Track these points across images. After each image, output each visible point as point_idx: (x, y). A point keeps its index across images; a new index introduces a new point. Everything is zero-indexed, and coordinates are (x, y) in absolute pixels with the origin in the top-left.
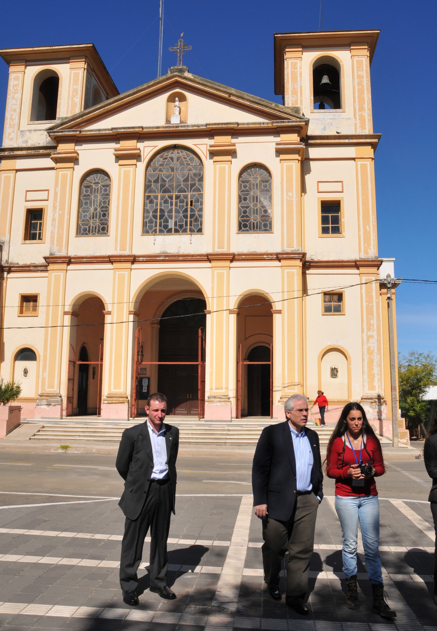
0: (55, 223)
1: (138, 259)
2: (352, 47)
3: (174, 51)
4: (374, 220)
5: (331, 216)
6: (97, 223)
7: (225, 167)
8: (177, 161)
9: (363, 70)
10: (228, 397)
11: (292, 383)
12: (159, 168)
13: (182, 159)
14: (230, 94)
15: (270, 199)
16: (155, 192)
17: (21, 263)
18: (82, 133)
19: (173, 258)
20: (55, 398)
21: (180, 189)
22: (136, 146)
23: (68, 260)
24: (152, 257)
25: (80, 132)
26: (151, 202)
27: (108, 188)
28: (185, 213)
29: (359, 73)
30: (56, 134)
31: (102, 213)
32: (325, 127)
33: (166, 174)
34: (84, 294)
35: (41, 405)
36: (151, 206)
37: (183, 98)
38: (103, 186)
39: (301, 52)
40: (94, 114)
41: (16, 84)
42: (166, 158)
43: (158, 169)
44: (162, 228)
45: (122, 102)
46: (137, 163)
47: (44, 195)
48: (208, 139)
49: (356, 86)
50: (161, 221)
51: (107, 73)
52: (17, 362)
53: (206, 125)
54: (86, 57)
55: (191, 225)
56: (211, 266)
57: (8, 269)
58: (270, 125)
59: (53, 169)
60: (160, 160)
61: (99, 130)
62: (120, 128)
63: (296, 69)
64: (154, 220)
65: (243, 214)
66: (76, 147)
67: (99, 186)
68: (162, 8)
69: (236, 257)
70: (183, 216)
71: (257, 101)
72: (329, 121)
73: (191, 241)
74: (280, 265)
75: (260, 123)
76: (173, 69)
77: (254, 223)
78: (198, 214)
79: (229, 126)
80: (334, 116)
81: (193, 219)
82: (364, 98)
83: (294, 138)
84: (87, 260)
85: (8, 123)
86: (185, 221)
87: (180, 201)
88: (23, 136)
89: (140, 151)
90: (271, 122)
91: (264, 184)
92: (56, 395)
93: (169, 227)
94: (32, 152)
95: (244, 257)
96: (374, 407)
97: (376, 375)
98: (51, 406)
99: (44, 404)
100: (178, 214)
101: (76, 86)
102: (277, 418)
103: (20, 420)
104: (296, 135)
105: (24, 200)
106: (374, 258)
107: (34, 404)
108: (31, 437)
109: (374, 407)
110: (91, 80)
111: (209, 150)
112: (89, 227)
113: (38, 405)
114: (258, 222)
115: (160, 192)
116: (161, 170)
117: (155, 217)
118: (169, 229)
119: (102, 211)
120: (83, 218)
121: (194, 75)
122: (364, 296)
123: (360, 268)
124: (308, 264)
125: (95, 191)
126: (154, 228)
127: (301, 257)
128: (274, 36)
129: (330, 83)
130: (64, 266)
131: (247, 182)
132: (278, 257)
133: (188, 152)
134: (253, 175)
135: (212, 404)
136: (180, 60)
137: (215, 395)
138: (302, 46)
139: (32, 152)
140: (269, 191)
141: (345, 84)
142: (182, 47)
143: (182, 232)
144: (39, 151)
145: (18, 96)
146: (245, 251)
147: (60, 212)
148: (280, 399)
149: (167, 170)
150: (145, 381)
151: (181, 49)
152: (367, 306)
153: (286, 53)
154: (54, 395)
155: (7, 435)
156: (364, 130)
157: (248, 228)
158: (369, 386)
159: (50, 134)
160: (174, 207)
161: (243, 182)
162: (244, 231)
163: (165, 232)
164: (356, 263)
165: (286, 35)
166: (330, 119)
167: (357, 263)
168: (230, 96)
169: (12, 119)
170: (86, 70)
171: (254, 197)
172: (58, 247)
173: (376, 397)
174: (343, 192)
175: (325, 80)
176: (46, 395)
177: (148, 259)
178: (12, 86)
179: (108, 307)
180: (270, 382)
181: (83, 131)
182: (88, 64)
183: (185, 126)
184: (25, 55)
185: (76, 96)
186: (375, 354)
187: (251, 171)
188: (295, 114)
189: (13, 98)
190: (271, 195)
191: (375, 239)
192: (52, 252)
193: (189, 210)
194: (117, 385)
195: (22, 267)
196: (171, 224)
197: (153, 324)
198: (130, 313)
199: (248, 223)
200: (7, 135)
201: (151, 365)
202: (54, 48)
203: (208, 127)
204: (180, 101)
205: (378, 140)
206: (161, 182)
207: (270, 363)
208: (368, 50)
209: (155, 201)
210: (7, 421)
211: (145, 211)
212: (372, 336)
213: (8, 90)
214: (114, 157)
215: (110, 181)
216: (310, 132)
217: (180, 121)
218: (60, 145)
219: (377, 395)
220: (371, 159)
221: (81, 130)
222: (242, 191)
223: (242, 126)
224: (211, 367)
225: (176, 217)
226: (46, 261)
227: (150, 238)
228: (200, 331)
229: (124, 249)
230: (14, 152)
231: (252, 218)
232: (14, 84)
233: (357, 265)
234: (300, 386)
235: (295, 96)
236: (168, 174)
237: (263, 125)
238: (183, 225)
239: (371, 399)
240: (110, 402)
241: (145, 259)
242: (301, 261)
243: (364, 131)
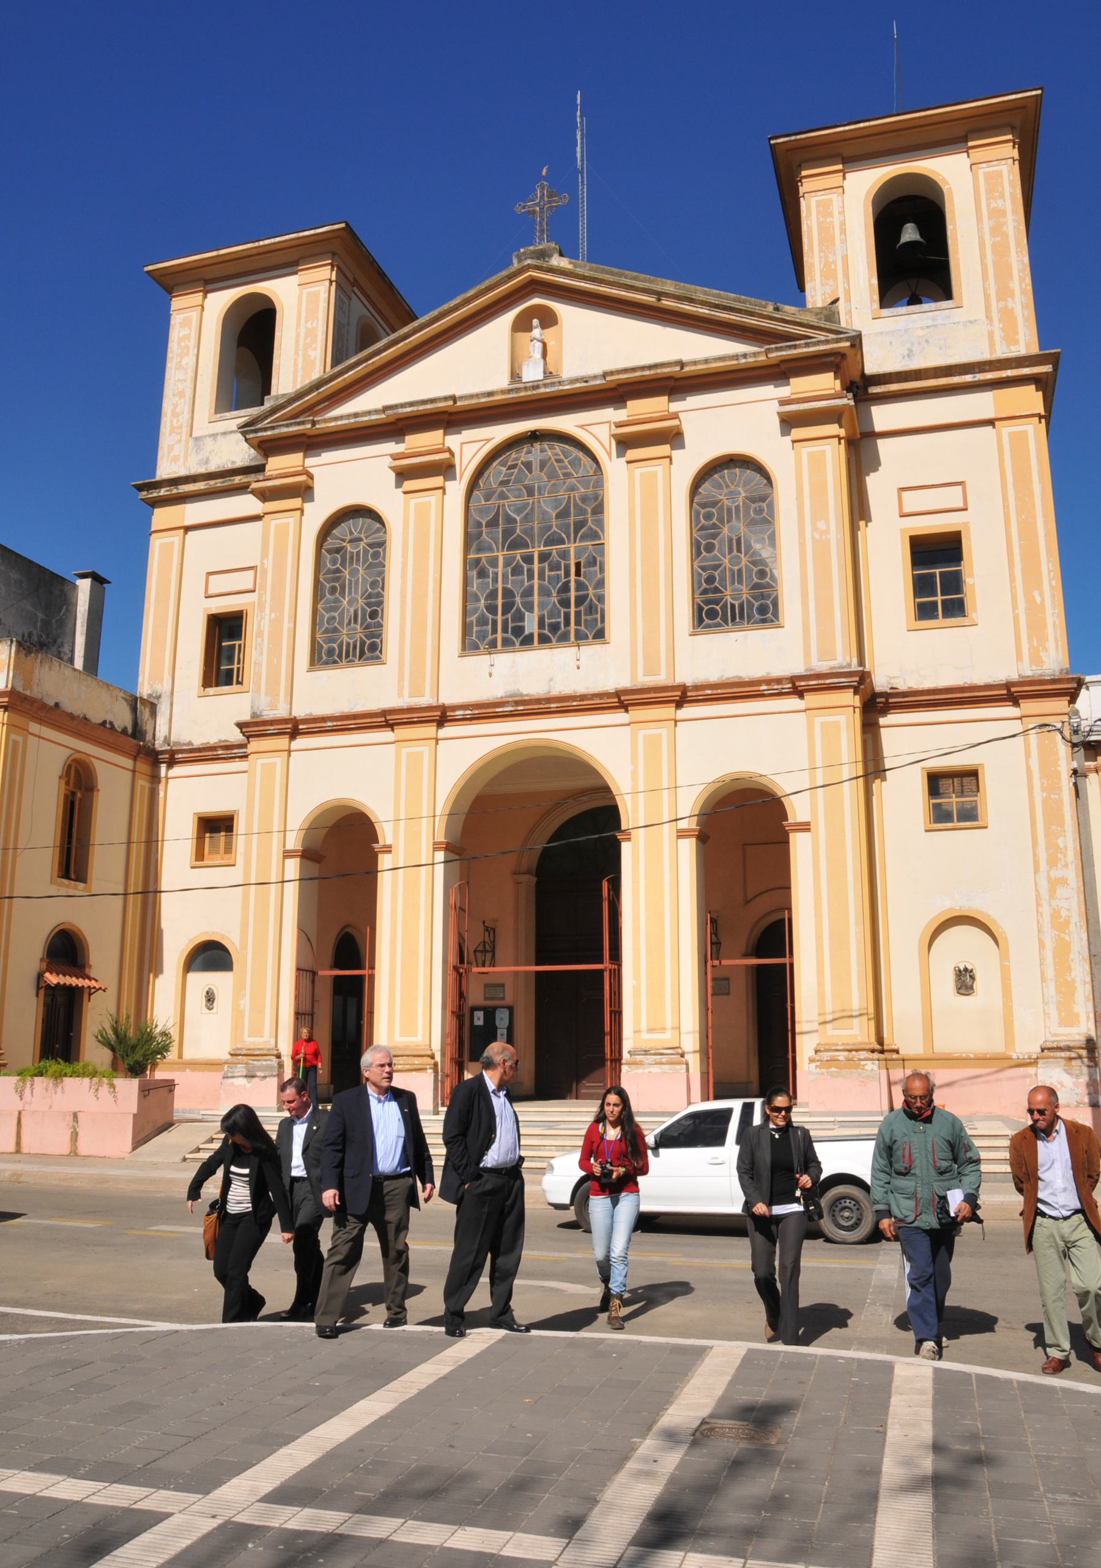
0: (263, 641)
1: (452, 714)
2: (970, 144)
3: (529, 212)
4: (1052, 574)
5: (940, 573)
6: (358, 635)
7: (656, 472)
8: (541, 470)
9: (1002, 196)
10: (680, 1051)
11: (843, 1011)
12: (500, 489)
13: (552, 464)
14: (660, 295)
15: (772, 540)
16: (490, 549)
17: (197, 742)
19: (536, 707)
20: (265, 1060)
21: (548, 537)
22: (443, 444)
23: (290, 726)
24: (484, 708)
25: (314, 423)
26: (482, 574)
27: (380, 550)
28: (564, 595)
29: (993, 205)
30: (260, 434)
31: (369, 610)
32: (910, 351)
34: (335, 804)
35: (232, 1077)
36: (482, 583)
37: (548, 319)
38: (371, 545)
39: (842, 174)
40: (344, 379)
42: (514, 466)
43: (496, 495)
44: (509, 635)
45: (407, 344)
46: (447, 483)
47: (244, 580)
49: (987, 237)
50: (507, 619)
51: (391, 286)
52: (192, 976)
53: (605, 375)
54: (334, 254)
55: (578, 622)
56: (627, 721)
57: (167, 756)
58: (763, 358)
59: (257, 518)
61: (356, 415)
62: (403, 405)
63: (831, 215)
64: (490, 616)
65: (704, 585)
66: (307, 460)
67: (361, 547)
68: (582, 148)
69: (689, 694)
70: (559, 602)
71: (725, 302)
72: (921, 333)
73: (578, 663)
74: (803, 708)
75: (736, 357)
76: (524, 253)
77: (733, 606)
78: (595, 595)
79: (659, 371)
80: (934, 319)
81: (582, 608)
82: (1009, 267)
83: (825, 383)
84: (335, 723)
85: (168, 425)
86: (565, 613)
87: (549, 565)
88: (198, 449)
89: (452, 454)
90: (763, 350)
91: (757, 505)
92: (268, 1053)
93: (527, 632)
94: (218, 483)
95: (709, 692)
96: (1078, 1072)
97: (1078, 984)
98: (256, 1079)
99: (240, 1074)
100: (546, 598)
102: (807, 1105)
103: (173, 1116)
104: (831, 375)
105: (203, 595)
106: (1057, 673)
107: (217, 1076)
108: (188, 1156)
109: (1078, 1072)
110: (349, 306)
111: (614, 436)
112: (340, 646)
113: (228, 1077)
114: (743, 602)
116: (502, 496)
117: (492, 609)
119: (369, 605)
120: (326, 625)
121: (573, 261)
122: (1036, 775)
123: (1020, 701)
124: (883, 700)
125: (352, 558)
126: (490, 637)
127: (855, 684)
128: (770, 144)
129: (922, 240)
130: (283, 742)
131: (714, 504)
132: (796, 687)
133: (567, 446)
134: (728, 486)
135: (640, 1071)
136: (542, 231)
137: (645, 1046)
138: (843, 159)
139: (218, 483)
140: (768, 522)
141: (959, 236)
142: (546, 199)
143: (558, 641)
145: (190, 360)
146: (713, 676)
147: (273, 615)
148: (813, 1053)
149: (517, 493)
150: (503, 1016)
152: (1045, 802)
153: (803, 181)
155: (134, 1149)
157: (718, 619)
158: (1060, 1014)
159: (248, 436)
160: (536, 581)
161: (704, 505)
162: (708, 626)
163: (517, 644)
164: (1009, 690)
165: (799, 137)
166: (922, 328)
167: (1013, 689)
168: (659, 300)
169: (175, 414)
170: (334, 284)
171: (730, 540)
173: (1083, 1044)
174: (966, 509)
175: (910, 233)
176: (244, 1052)
177: (477, 712)
178: (176, 341)
179: (386, 834)
180: (787, 1009)
181: (318, 421)
182: (339, 270)
183: (554, 383)
185: (314, 346)
186: (1072, 927)
187: (723, 477)
188: (828, 325)
189: (179, 366)
190: (774, 532)
191: (1057, 623)
194: (408, 1027)
195: (199, 750)
196: (531, 625)
197: (519, 874)
198: (436, 847)
199: (718, 608)
200: (166, 450)
201: (516, 973)
202: (261, 243)
203: (608, 378)
204: (544, 326)
205: (1051, 366)
206: (503, 524)
207: (786, 960)
208: (1014, 144)
209: (491, 570)
210: (134, 1115)
211: (467, 597)
212: (1063, 881)
213: (169, 350)
214: (393, 475)
215: (385, 532)
216: (872, 367)
217: (545, 372)
218: (270, 459)
219: (1083, 1039)
220: (1037, 419)
221: (316, 419)
222: (703, 528)
223: (693, 368)
224: (636, 976)
225: (542, 605)
226: (241, 732)
227: (480, 662)
228: (605, 885)
229: (417, 691)
230: (180, 487)
232: (181, 335)
233: (1012, 694)
234: (865, 1018)
235: (831, 282)
236: (519, 502)
237: (743, 361)
238: (559, 623)
239: (1069, 1049)
241: (470, 712)
242: (855, 693)
243: (1013, 348)
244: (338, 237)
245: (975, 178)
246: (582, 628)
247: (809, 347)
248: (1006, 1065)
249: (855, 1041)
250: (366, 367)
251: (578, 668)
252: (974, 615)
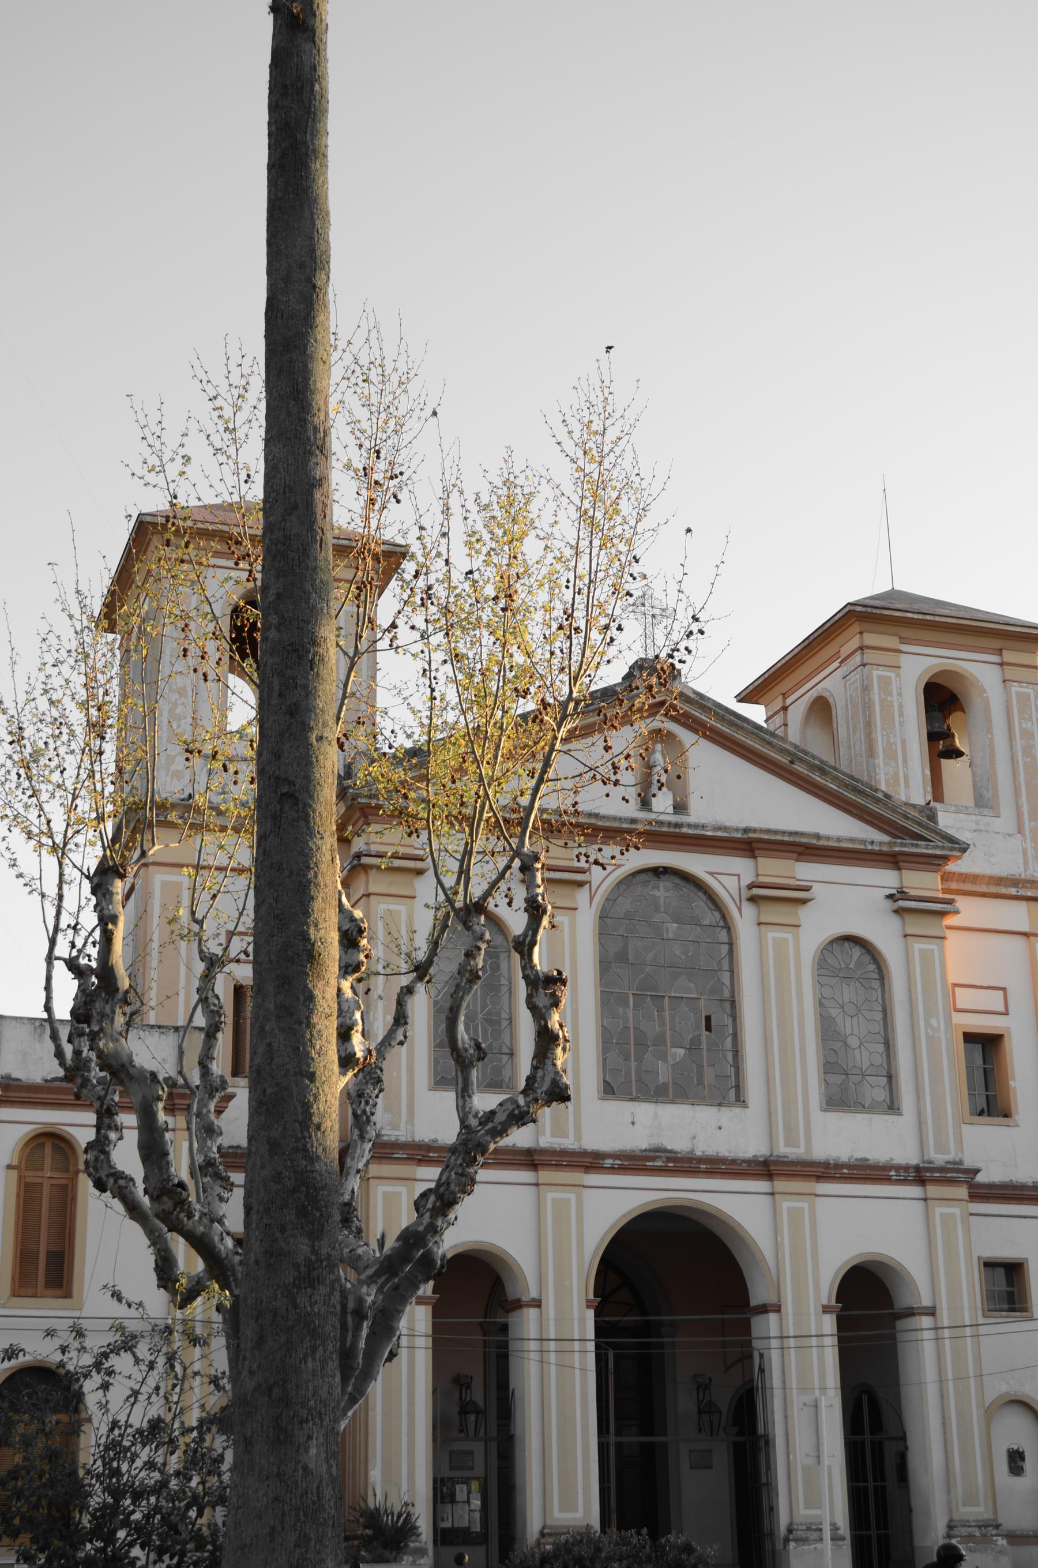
9: (1030, 719)
29: (1024, 726)
63: (891, 695)
75: (863, 842)
80: (977, 824)
135: (806, 1548)
166: (970, 831)
227: (620, 1110)
245: (1008, 694)
249: (981, 1518)
252: (1017, 1117)
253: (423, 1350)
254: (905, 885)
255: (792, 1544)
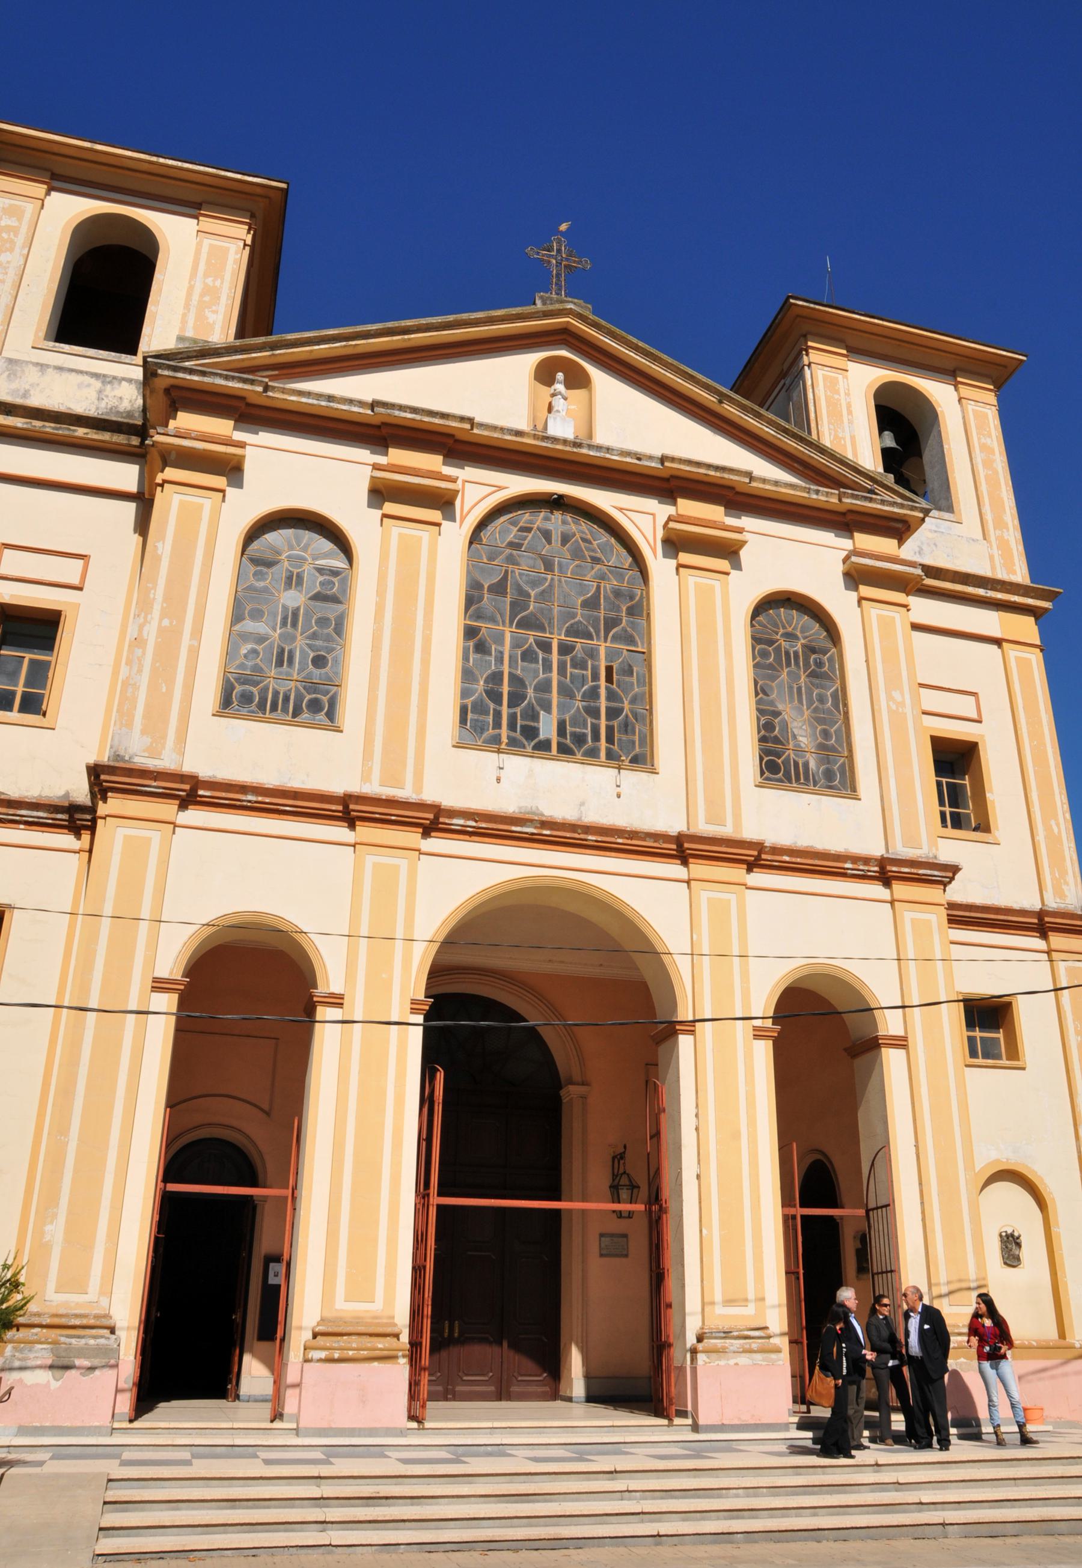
0: (144, 654)
1: (447, 821)
9: (990, 436)
11: (960, 1281)
16: (493, 620)
18: (270, 394)
19: (568, 835)
20: (95, 1337)
21: (572, 625)
24: (495, 822)
25: (266, 388)
26: (481, 648)
29: (983, 440)
30: (180, 375)
33: (527, 575)
35: (22, 1369)
40: (311, 351)
41: (7, 226)
42: (528, 530)
44: (518, 735)
45: (405, 340)
48: (656, 502)
50: (515, 713)
54: (252, 216)
55: (610, 739)
60: (509, 531)
61: (330, 398)
62: (401, 408)
64: (492, 706)
72: (930, 535)
77: (796, 764)
79: (726, 476)
87: (572, 660)
92: (98, 1323)
94: (49, 428)
95: (787, 858)
98: (73, 1372)
99: (39, 1362)
101: (214, 281)
113: (11, 1369)
115: (511, 623)
117: (496, 697)
118: (540, 742)
128: (786, 305)
135: (722, 1363)
136: (558, 284)
139: (49, 428)
144: (74, 431)
147: (166, 622)
149: (531, 562)
151: (562, 260)
154: (85, 1322)
156: (1013, 575)
163: (529, 749)
165: (817, 307)
167: (1047, 919)
168: (720, 402)
172: (148, 740)
176: (47, 1321)
177: (484, 825)
181: (274, 388)
184: (47, 156)
185: (214, 308)
187: (779, 616)
192: (122, 753)
193: (603, 692)
196: (547, 727)
202: (162, 160)
211: (467, 675)
221: (270, 384)
223: (761, 486)
225: (562, 708)
229: (392, 777)
231: (791, 747)
240: (336, 1356)
241: (473, 824)
244: (266, 197)
246: (616, 748)
247: (884, 505)
248: (1070, 1356)
250: (345, 346)
251: (619, 796)
253: (777, 1310)
254: (857, 546)
255: (701, 1358)
